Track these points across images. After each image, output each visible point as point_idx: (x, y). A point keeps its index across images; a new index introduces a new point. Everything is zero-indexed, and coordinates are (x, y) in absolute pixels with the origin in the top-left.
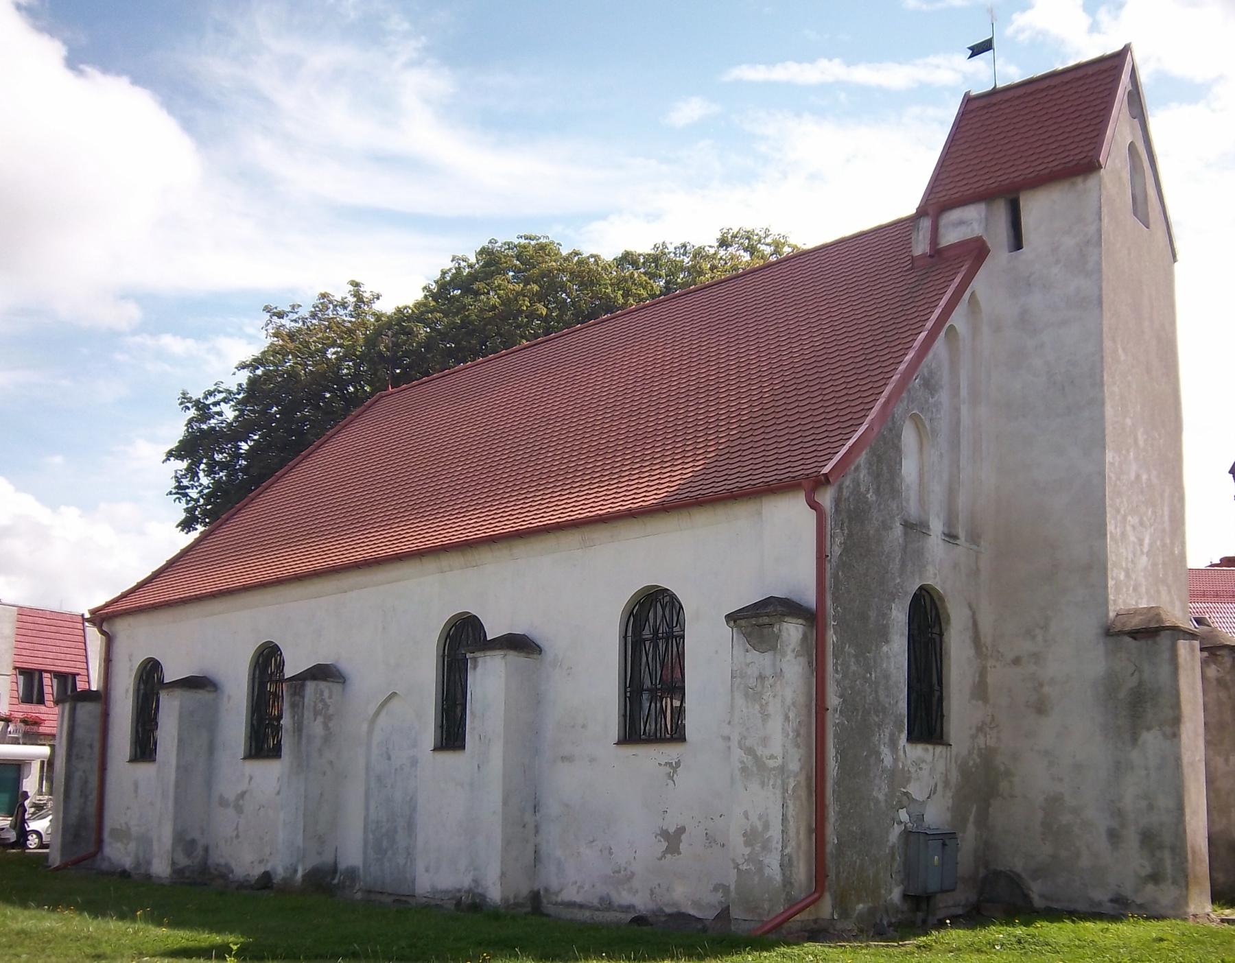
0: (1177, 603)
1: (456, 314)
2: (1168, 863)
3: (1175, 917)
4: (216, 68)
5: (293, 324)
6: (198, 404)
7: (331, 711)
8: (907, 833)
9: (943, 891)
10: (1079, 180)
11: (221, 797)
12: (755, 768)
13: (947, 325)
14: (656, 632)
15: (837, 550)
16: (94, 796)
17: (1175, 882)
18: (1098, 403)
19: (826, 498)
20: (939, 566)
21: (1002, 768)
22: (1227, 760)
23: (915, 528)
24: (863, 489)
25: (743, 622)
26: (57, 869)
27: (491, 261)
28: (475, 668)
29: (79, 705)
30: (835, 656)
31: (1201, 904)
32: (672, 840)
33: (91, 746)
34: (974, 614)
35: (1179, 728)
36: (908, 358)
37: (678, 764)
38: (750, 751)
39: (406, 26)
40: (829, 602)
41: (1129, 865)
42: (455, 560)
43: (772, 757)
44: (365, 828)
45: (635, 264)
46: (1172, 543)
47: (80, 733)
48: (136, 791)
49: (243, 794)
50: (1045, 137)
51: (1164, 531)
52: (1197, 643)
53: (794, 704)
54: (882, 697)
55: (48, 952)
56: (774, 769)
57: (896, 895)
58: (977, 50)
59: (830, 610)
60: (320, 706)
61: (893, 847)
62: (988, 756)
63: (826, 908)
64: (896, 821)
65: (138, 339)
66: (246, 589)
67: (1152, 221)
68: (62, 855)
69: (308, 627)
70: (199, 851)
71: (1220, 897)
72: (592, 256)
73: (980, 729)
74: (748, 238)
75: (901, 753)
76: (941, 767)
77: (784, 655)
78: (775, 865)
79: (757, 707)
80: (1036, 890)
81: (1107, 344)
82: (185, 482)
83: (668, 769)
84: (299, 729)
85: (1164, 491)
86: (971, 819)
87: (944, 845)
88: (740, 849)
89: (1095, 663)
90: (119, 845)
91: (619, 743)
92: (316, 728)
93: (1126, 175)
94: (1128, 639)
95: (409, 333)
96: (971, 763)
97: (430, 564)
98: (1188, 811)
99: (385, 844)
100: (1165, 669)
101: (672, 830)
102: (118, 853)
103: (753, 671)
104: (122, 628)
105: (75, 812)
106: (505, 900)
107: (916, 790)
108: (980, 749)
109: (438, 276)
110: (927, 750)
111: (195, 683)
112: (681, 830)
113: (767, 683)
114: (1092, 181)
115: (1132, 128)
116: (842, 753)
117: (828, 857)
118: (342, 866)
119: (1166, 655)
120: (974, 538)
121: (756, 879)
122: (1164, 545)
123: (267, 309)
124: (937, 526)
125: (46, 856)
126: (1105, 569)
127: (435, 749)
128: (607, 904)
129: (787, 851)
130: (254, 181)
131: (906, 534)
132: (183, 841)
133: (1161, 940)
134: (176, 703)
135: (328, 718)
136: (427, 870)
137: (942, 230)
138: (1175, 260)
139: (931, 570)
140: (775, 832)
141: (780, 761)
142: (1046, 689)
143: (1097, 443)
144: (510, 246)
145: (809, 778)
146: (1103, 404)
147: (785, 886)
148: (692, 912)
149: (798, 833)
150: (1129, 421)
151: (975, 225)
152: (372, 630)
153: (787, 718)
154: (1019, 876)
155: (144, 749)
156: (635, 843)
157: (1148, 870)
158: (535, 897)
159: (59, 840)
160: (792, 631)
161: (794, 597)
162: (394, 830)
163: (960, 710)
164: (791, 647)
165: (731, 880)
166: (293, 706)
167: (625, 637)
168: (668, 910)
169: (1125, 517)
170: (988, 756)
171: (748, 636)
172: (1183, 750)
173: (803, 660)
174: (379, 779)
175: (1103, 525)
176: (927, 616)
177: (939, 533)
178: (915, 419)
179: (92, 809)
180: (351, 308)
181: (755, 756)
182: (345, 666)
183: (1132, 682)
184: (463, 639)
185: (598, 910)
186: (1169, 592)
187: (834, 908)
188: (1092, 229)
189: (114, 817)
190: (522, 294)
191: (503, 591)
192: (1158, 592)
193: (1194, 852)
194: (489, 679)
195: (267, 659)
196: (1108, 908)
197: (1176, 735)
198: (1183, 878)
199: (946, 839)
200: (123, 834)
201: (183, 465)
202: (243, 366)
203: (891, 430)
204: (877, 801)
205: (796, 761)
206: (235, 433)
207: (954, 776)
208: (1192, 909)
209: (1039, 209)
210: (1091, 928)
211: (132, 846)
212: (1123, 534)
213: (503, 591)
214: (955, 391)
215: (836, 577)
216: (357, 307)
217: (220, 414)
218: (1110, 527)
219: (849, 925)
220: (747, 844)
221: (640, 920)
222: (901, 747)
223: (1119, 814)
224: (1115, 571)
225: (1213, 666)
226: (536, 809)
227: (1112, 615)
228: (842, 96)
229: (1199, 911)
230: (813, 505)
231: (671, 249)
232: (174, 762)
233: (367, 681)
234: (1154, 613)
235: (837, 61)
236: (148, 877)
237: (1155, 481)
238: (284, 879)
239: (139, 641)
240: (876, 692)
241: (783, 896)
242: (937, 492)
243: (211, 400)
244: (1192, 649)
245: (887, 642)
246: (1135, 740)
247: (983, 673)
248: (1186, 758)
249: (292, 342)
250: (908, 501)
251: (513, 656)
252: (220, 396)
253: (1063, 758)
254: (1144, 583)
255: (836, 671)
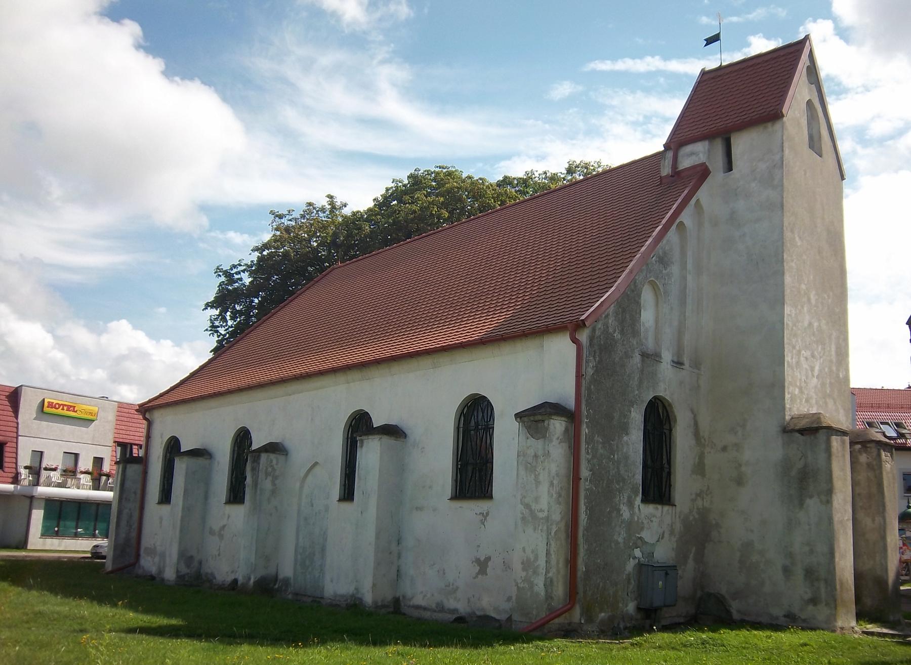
0: (842, 411)
1: (389, 217)
2: (823, 590)
3: (828, 629)
4: (262, 65)
5: (289, 222)
6: (227, 274)
7: (277, 473)
8: (640, 566)
9: (665, 606)
10: (769, 124)
11: (211, 528)
12: (530, 517)
13: (678, 221)
14: (477, 424)
15: (590, 371)
16: (135, 526)
17: (827, 604)
18: (780, 273)
19: (584, 336)
20: (668, 383)
21: (714, 522)
22: (873, 520)
23: (651, 357)
24: (611, 330)
25: (526, 419)
26: (111, 572)
27: (416, 181)
28: (362, 447)
29: (128, 466)
30: (587, 443)
31: (847, 621)
32: (483, 565)
33: (135, 493)
34: (695, 416)
35: (831, 497)
36: (648, 243)
37: (488, 514)
38: (527, 506)
39: (381, 37)
40: (583, 407)
41: (797, 591)
42: (355, 375)
43: (541, 511)
44: (296, 551)
45: (510, 183)
46: (838, 370)
47: (128, 484)
48: (161, 523)
49: (224, 526)
50: (750, 99)
51: (831, 361)
52: (847, 439)
53: (557, 475)
54: (622, 472)
55: (50, 627)
56: (542, 519)
57: (631, 607)
58: (710, 41)
59: (584, 412)
60: (270, 469)
61: (629, 574)
62: (704, 514)
63: (577, 615)
64: (632, 556)
65: (213, 234)
66: (230, 392)
67: (824, 152)
68: (113, 564)
69: (270, 416)
70: (196, 564)
71: (861, 616)
72: (481, 179)
73: (698, 495)
74: (586, 168)
75: (637, 510)
76: (668, 520)
77: (551, 441)
78: (541, 585)
79: (533, 476)
80: (735, 606)
81: (788, 234)
82: (217, 323)
83: (481, 517)
84: (255, 484)
85: (831, 334)
86: (691, 556)
87: (667, 574)
88: (519, 573)
89: (776, 451)
90: (149, 558)
91: (452, 499)
92: (267, 484)
93: (804, 122)
94: (797, 435)
95: (360, 229)
96: (691, 518)
97: (341, 378)
98: (837, 555)
99: (307, 563)
100: (822, 456)
101: (482, 559)
102: (148, 564)
103: (531, 452)
104: (158, 417)
105: (123, 535)
106: (375, 602)
107: (646, 535)
108: (698, 509)
109: (384, 192)
110: (657, 509)
111: (196, 453)
112: (488, 559)
113: (539, 461)
114: (778, 126)
115: (810, 90)
116: (590, 509)
117: (579, 580)
118: (281, 576)
119: (823, 446)
120: (696, 364)
121: (529, 594)
122: (831, 371)
123: (272, 213)
124: (667, 356)
125: (103, 564)
126: (784, 387)
127: (340, 500)
128: (441, 608)
129: (550, 575)
130: (288, 136)
131: (643, 361)
132: (185, 557)
133: (805, 645)
134: (184, 466)
135: (275, 478)
136: (332, 581)
137: (680, 159)
138: (843, 178)
139: (662, 386)
140: (542, 562)
141: (546, 514)
142: (743, 469)
143: (779, 301)
144: (429, 173)
145: (567, 525)
146: (783, 274)
147: (547, 599)
148: (493, 615)
149: (558, 563)
150: (803, 287)
151: (701, 155)
152: (305, 419)
153: (552, 484)
154: (723, 597)
155: (166, 497)
156: (460, 567)
157: (808, 596)
158: (397, 601)
159: (112, 553)
160: (558, 425)
161: (563, 404)
162: (312, 554)
163: (683, 481)
164: (557, 436)
165: (513, 592)
166: (253, 469)
167: (458, 428)
168: (478, 613)
169: (799, 352)
170: (704, 514)
171: (528, 428)
172: (834, 512)
173: (565, 446)
174: (306, 519)
175: (782, 357)
176: (658, 418)
177: (669, 361)
178: (653, 284)
179: (134, 534)
180: (328, 212)
181: (531, 510)
182: (288, 444)
183: (800, 465)
184: (360, 426)
185: (435, 611)
186: (835, 403)
187: (582, 615)
188: (777, 157)
189: (146, 542)
190: (432, 203)
191: (388, 396)
192: (826, 403)
193: (842, 584)
194: (371, 452)
195: (243, 437)
196: (782, 621)
197: (829, 502)
198: (833, 602)
199: (668, 570)
200: (152, 552)
201: (217, 312)
202: (256, 249)
203: (633, 291)
204: (617, 543)
205: (558, 514)
206: (253, 290)
207: (678, 526)
208: (839, 624)
209: (742, 143)
210: (760, 637)
211: (157, 559)
212: (798, 363)
213: (388, 396)
214: (684, 266)
215: (589, 389)
216: (331, 211)
217: (241, 279)
218: (788, 358)
219: (589, 628)
220: (524, 569)
221: (460, 620)
222: (636, 506)
223: (790, 555)
224: (791, 388)
225: (864, 455)
226: (399, 543)
227: (788, 418)
228: (662, 80)
229: (846, 625)
230: (574, 340)
231: (537, 175)
232: (181, 503)
233: (301, 455)
234: (817, 417)
235: (657, 57)
236: (163, 580)
237: (824, 327)
238: (242, 584)
239: (167, 425)
240: (618, 468)
241: (546, 606)
242: (668, 334)
243: (235, 270)
244: (843, 442)
245: (627, 434)
246: (801, 504)
247: (701, 457)
248: (837, 517)
249: (286, 234)
250: (646, 339)
251: (386, 440)
252: (241, 268)
253: (754, 516)
254: (815, 396)
255: (588, 453)
